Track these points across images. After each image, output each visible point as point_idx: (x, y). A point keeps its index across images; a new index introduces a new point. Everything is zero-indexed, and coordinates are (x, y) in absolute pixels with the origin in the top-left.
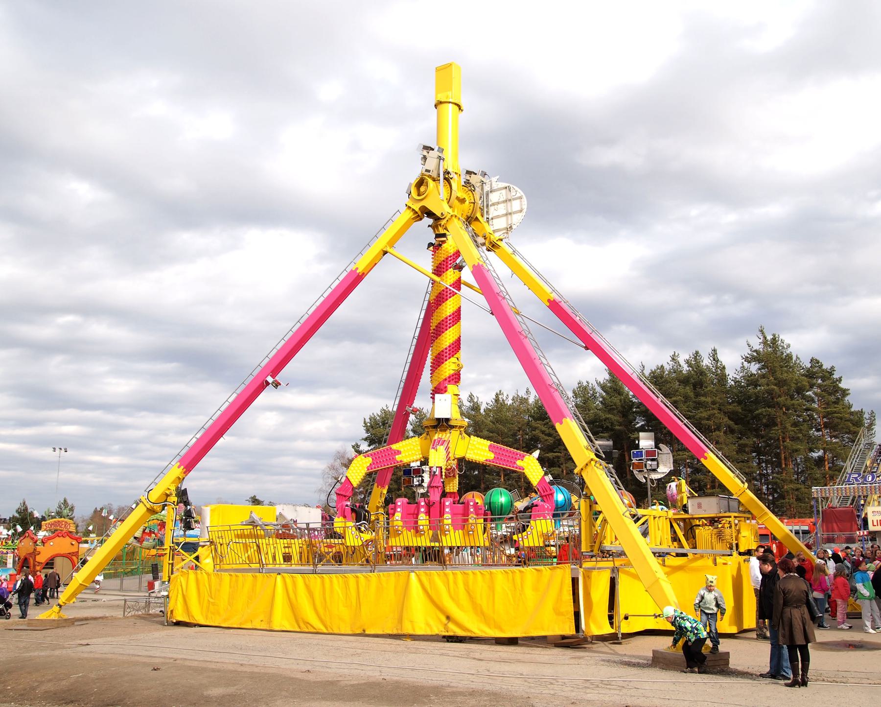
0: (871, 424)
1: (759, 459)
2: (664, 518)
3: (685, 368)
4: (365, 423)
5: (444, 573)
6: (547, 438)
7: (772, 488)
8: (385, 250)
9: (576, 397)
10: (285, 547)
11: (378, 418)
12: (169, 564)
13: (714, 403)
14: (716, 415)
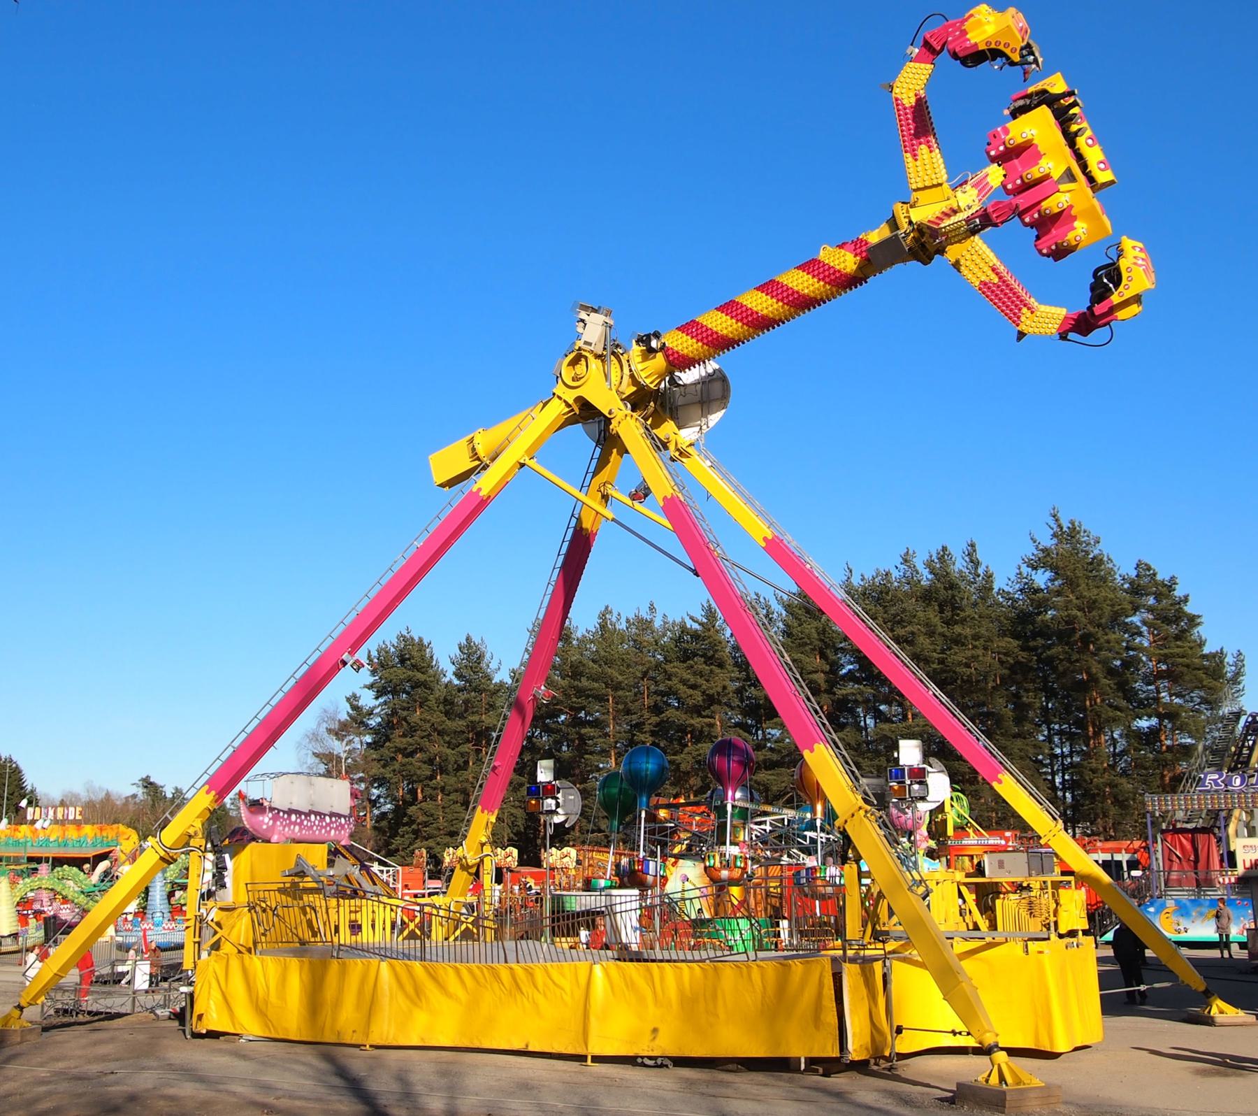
0: (1238, 674)
2: (950, 882)
3: (926, 577)
6: (690, 692)
7: (1072, 779)
8: (522, 461)
11: (393, 650)
12: (195, 943)
13: (976, 637)
14: (981, 658)
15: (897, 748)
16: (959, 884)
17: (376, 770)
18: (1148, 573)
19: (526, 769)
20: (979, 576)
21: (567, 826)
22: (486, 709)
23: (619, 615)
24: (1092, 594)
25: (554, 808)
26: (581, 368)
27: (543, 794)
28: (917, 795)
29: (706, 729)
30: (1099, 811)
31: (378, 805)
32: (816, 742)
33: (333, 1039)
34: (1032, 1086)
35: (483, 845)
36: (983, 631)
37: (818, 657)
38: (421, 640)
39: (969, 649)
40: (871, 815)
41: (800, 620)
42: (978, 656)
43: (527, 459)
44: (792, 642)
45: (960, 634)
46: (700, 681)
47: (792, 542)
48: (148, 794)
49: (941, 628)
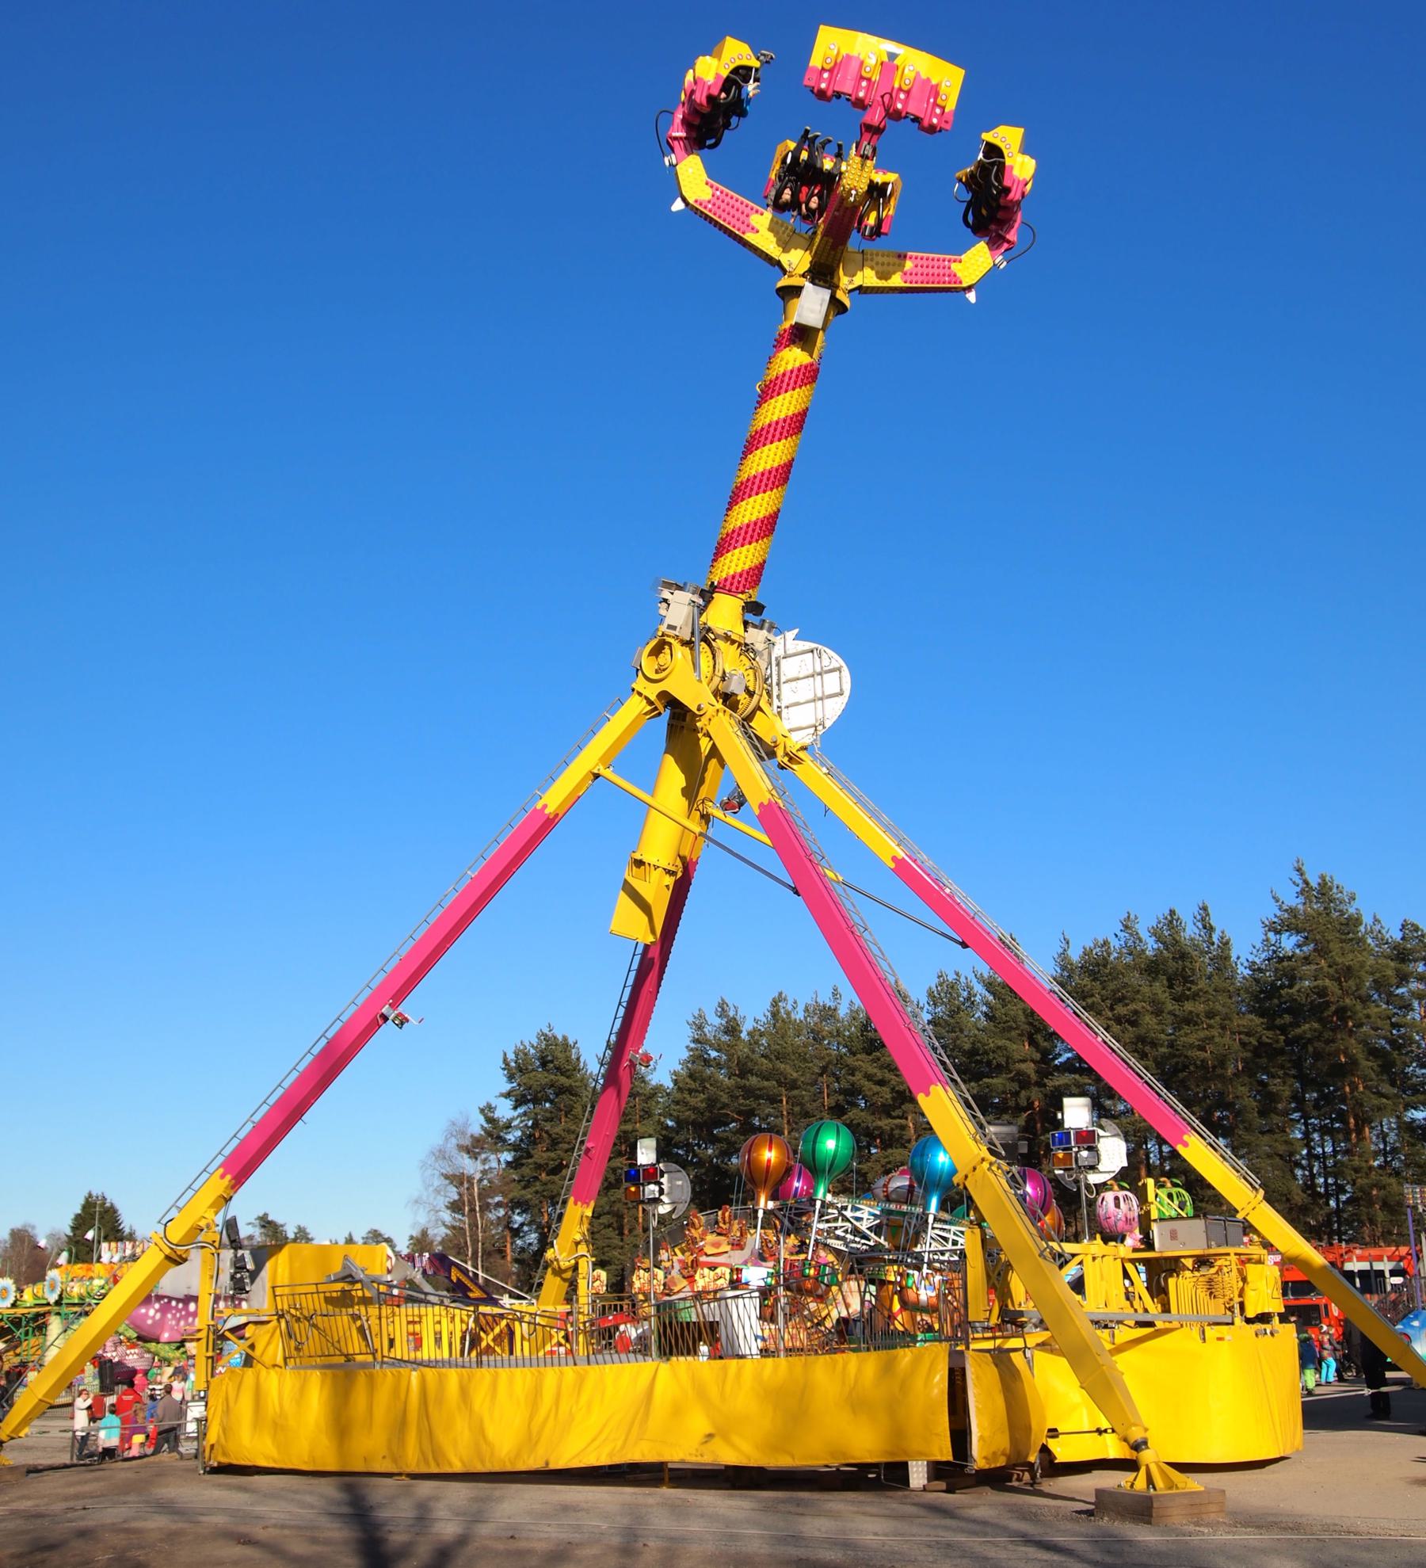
1: (1306, 1124)
2: (1112, 1258)
3: (1151, 946)
4: (505, 1060)
5: (439, 1373)
6: (877, 1088)
7: (1335, 1183)
8: (596, 771)
9: (935, 1004)
10: (409, 1323)
11: (532, 1051)
13: (1210, 1015)
14: (1217, 1040)
15: (1061, 1108)
16: (1123, 1260)
17: (517, 1192)
18: (1415, 935)
19: (627, 1146)
20: (1213, 944)
21: (674, 1217)
22: (640, 1116)
23: (795, 1002)
24: (1347, 960)
25: (657, 1196)
26: (664, 658)
27: (644, 1179)
28: (1086, 1163)
29: (897, 1132)
30: (1364, 1217)
31: (521, 1235)
32: (932, 1083)
33: (360, 1467)
34: (1186, 1490)
35: (577, 1243)
36: (1219, 1007)
37: (1026, 1044)
38: (565, 1038)
39: (1203, 1029)
40: (998, 1168)
41: (1004, 1000)
42: (1213, 1037)
43: (601, 767)
44: (995, 1026)
45: (1191, 1012)
46: (888, 1076)
47: (927, 863)
48: (267, 1235)
49: (1170, 1006)
